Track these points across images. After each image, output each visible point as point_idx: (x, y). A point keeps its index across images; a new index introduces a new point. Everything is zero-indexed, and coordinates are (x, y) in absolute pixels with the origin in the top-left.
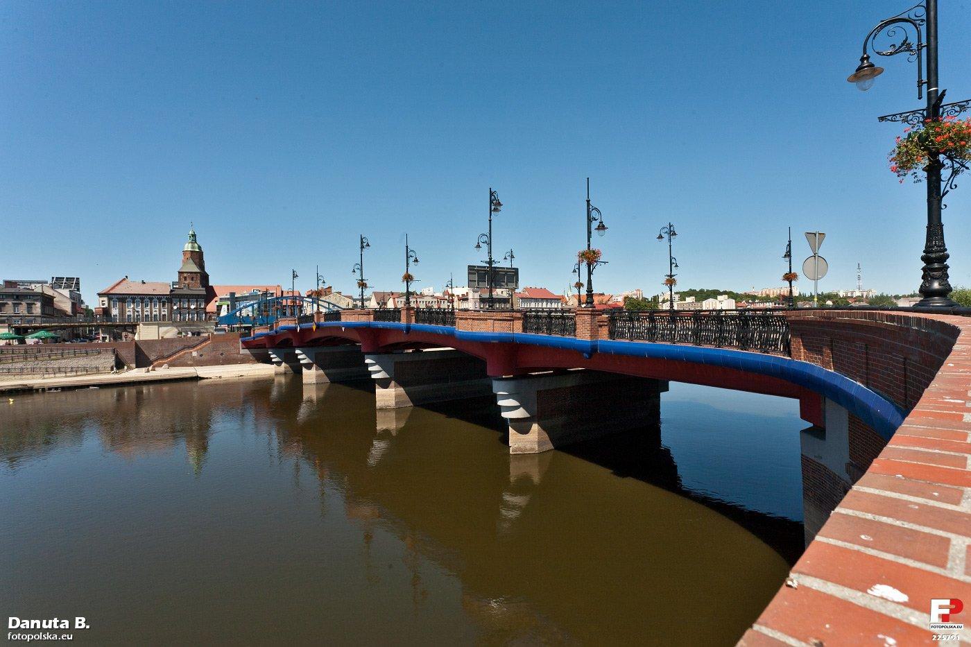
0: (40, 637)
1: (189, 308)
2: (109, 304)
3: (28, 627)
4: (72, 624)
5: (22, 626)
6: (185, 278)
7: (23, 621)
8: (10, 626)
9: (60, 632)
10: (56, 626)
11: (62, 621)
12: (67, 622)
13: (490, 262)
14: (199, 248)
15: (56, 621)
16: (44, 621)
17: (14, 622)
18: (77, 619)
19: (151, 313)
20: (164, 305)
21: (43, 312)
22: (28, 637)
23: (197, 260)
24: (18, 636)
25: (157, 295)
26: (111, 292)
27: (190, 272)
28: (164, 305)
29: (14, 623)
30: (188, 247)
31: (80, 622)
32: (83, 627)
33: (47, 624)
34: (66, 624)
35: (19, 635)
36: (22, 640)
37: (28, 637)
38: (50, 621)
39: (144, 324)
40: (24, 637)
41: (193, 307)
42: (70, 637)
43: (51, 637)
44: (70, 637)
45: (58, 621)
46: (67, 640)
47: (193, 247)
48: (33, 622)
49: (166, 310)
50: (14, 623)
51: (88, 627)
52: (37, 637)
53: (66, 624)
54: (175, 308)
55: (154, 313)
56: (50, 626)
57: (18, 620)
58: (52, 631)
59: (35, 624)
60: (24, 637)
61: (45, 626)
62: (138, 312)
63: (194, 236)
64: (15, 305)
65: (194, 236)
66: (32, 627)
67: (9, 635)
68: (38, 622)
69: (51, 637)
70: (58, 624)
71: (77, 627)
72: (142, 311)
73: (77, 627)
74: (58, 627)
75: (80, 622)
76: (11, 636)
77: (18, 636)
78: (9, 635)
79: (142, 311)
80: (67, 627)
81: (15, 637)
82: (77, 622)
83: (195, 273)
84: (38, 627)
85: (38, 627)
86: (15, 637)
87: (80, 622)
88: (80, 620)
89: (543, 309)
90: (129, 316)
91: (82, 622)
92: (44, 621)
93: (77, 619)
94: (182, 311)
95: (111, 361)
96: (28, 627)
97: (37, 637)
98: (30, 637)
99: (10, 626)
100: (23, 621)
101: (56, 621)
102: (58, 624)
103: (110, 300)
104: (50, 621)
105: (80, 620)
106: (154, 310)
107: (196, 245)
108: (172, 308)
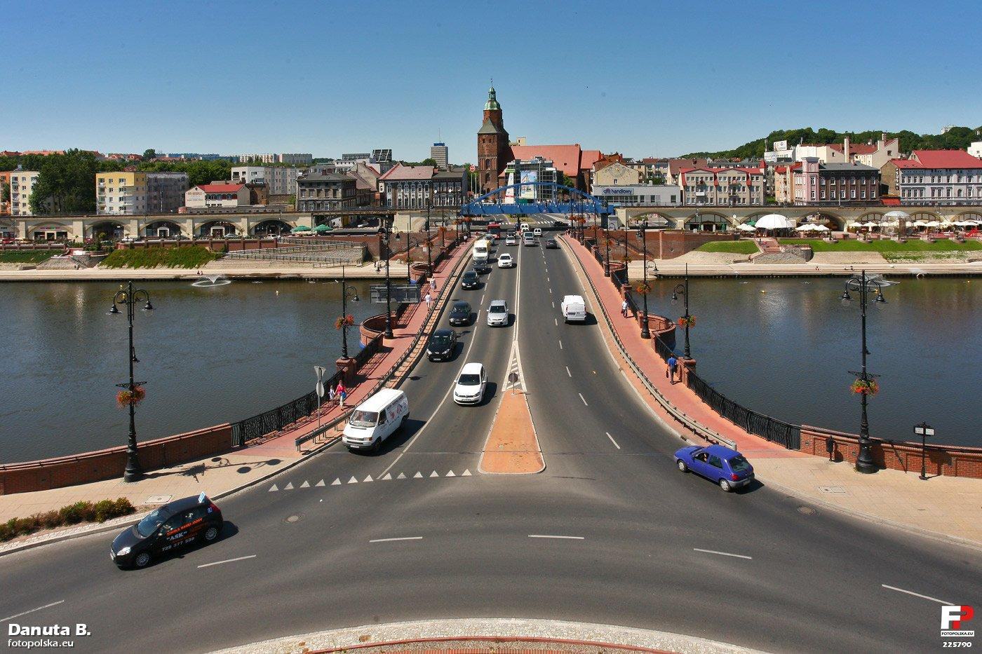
0: (40, 644)
1: (447, 192)
2: (385, 190)
3: (28, 634)
4: (73, 630)
5: (23, 633)
6: (484, 140)
7: (23, 628)
8: (10, 633)
9: (60, 638)
10: (56, 633)
11: (63, 628)
12: (68, 629)
13: (195, 477)
14: (498, 105)
15: (56, 627)
16: (45, 628)
17: (14, 629)
18: (78, 625)
19: (417, 197)
20: (427, 190)
21: (343, 197)
22: (28, 644)
23: (496, 120)
24: (18, 643)
25: (408, 180)
26: (387, 178)
27: (488, 134)
28: (427, 190)
29: (14, 629)
30: (487, 107)
31: (81, 629)
32: (84, 633)
33: (48, 630)
34: (67, 631)
35: (19, 642)
36: (22, 647)
37: (28, 644)
38: (51, 628)
39: (400, 214)
40: (25, 644)
41: (450, 191)
42: (70, 644)
43: (52, 644)
44: (70, 644)
45: (59, 628)
46: (68, 647)
47: (492, 106)
48: (33, 629)
49: (428, 194)
50: (14, 629)
51: (89, 634)
52: (37, 644)
53: (67, 631)
54: (436, 192)
55: (419, 197)
56: (50, 633)
57: (18, 627)
58: (52, 637)
59: (36, 631)
60: (25, 644)
61: (45, 633)
62: (406, 196)
63: (493, 93)
64: (327, 191)
65: (493, 93)
66: (33, 634)
67: (9, 642)
68: (38, 629)
69: (52, 644)
70: (59, 631)
71: (78, 633)
72: (410, 195)
73: (78, 633)
74: (58, 634)
75: (81, 629)
76: (11, 643)
77: (18, 643)
78: (9, 642)
79: (410, 195)
80: (68, 634)
81: (15, 644)
82: (78, 629)
83: (493, 134)
84: (39, 633)
85: (39, 633)
86: (15, 644)
87: (81, 629)
88: (81, 627)
89: (910, 202)
90: (400, 200)
91: (83, 629)
92: (45, 628)
93: (78, 625)
94: (442, 195)
95: (360, 255)
96: (28, 634)
97: (37, 644)
98: (31, 644)
99: (10, 633)
100: (23, 628)
101: (56, 627)
102: (59, 631)
103: (386, 185)
104: (51, 628)
105: (81, 627)
106: (419, 194)
107: (495, 103)
108: (433, 192)
